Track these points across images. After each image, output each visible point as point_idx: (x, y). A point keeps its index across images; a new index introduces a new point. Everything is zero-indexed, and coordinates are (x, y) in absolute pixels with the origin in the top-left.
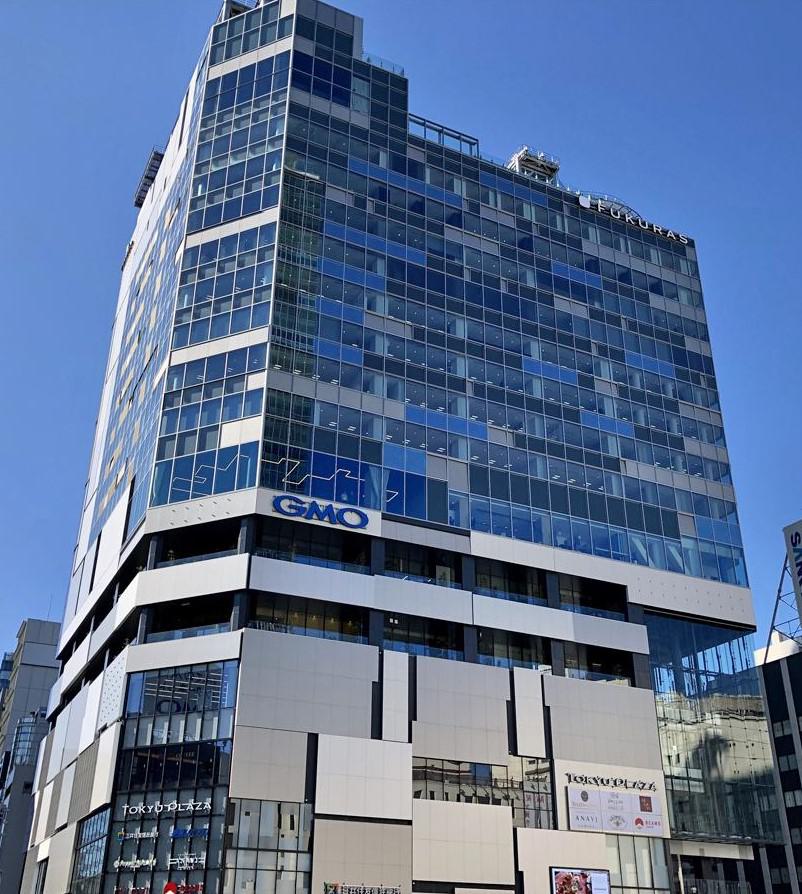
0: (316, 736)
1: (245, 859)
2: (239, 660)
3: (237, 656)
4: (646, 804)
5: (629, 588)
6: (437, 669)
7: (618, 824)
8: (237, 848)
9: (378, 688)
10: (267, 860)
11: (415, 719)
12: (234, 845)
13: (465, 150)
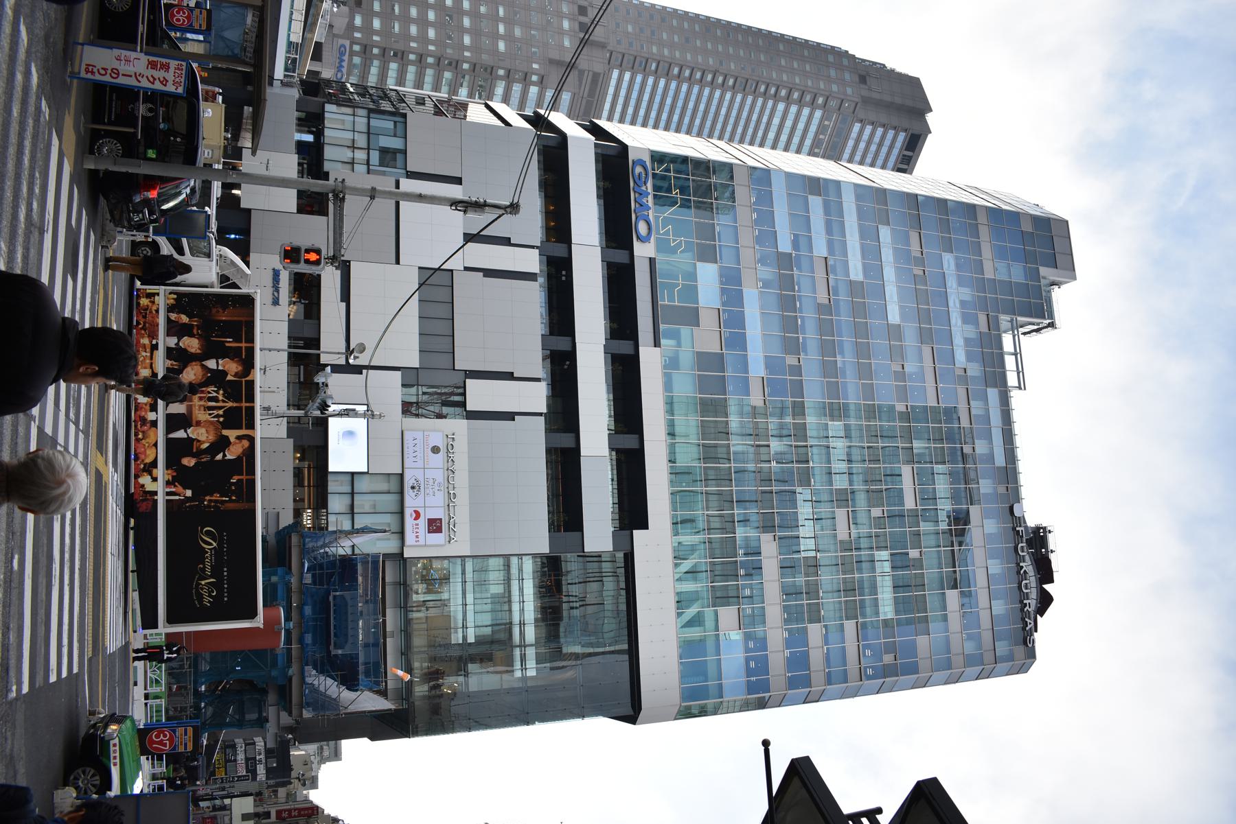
0: (460, 183)
1: (361, 122)
2: (454, 369)
3: (456, 368)
4: (434, 526)
5: (938, 778)
6: (533, 297)
7: (413, 488)
8: (369, 118)
9: (489, 273)
10: (361, 141)
11: (484, 276)
12: (372, 115)
13: (1012, 379)
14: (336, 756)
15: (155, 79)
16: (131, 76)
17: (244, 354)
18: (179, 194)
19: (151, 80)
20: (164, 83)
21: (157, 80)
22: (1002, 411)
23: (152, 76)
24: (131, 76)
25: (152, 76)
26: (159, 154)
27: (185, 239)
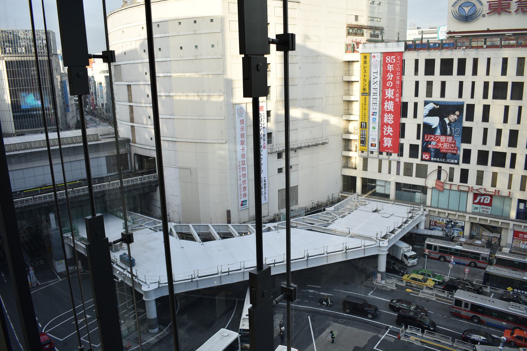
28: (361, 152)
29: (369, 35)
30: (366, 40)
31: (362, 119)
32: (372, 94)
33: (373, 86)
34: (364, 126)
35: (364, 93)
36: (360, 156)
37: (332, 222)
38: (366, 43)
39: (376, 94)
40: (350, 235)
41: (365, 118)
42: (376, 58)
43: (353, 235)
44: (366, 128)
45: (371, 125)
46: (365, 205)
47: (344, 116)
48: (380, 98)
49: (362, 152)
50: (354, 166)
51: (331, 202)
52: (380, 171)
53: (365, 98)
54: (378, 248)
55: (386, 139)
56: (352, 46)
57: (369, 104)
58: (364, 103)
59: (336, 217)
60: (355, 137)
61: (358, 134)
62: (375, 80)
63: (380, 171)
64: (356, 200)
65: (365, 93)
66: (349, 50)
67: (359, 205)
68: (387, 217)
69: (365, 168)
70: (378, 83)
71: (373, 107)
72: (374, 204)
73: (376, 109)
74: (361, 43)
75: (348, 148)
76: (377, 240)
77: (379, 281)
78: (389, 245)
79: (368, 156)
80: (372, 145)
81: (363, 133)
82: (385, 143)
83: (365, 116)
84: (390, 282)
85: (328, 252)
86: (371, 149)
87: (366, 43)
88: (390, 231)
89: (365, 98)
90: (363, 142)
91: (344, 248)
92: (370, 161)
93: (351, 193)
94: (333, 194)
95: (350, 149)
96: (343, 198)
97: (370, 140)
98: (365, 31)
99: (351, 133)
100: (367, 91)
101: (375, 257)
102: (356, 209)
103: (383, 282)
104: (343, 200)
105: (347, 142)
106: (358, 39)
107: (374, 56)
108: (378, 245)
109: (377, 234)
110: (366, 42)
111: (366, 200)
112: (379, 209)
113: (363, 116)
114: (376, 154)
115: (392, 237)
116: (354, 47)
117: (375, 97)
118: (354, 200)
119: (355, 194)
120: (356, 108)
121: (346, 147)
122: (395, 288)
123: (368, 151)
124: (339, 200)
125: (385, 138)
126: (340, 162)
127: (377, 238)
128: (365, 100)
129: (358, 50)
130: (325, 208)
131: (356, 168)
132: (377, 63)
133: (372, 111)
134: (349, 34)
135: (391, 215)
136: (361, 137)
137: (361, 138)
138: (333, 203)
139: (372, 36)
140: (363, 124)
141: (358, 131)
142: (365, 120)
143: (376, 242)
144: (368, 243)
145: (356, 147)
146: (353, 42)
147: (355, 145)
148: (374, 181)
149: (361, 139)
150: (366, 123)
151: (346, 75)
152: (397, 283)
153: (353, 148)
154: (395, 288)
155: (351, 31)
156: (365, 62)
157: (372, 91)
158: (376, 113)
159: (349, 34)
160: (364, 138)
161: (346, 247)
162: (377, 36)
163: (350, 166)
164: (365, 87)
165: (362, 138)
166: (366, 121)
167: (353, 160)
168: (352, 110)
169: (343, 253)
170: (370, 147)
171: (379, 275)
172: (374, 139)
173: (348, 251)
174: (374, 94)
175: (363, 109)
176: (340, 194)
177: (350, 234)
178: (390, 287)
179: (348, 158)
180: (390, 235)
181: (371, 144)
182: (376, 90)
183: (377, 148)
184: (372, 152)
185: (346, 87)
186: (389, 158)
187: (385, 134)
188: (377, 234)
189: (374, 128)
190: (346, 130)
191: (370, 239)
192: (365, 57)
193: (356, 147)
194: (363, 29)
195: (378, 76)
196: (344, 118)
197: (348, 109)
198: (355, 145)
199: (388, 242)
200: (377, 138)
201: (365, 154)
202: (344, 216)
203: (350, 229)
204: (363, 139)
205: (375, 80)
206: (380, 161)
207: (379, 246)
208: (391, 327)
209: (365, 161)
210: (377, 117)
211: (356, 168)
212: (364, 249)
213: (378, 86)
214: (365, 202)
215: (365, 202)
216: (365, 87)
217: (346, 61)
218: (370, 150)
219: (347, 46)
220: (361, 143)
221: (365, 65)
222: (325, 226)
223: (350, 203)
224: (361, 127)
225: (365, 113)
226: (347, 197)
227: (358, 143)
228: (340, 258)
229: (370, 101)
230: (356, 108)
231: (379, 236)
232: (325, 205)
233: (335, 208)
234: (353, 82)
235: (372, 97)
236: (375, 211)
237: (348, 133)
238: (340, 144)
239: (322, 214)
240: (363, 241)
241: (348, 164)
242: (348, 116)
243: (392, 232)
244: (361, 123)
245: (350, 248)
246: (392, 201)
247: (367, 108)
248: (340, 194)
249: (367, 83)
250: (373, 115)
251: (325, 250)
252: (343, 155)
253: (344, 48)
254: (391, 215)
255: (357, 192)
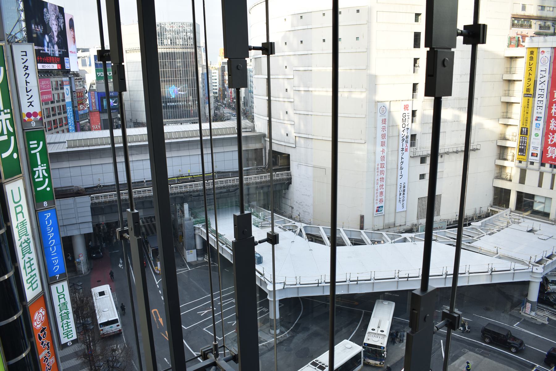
14: (263, 44)
15: (26, 74)
16: (24, 217)
17: (134, 278)
18: (262, 345)
19: (27, 75)
20: (26, 67)
21: (26, 72)
22: (363, 223)
23: (25, 75)
24: (24, 217)
25: (25, 75)
26: (282, 319)
27: (3, 155)
28: (518, 162)
29: (538, 27)
30: (534, 33)
31: (523, 124)
32: (537, 96)
33: (538, 87)
34: (524, 132)
35: (528, 94)
36: (518, 167)
37: (477, 238)
38: (533, 37)
39: (542, 96)
40: (498, 255)
41: (527, 123)
42: (545, 54)
43: (501, 256)
44: (527, 134)
45: (534, 132)
46: (519, 223)
47: (501, 120)
48: (547, 101)
49: (520, 162)
50: (508, 177)
51: (479, 217)
52: (540, 185)
53: (528, 100)
54: (531, 274)
55: (551, 148)
56: (517, 39)
57: (533, 107)
58: (527, 106)
59: (482, 233)
60: (513, 144)
61: (517, 141)
62: (542, 80)
63: (540, 185)
64: (509, 217)
65: (529, 94)
66: (512, 44)
67: (511, 222)
68: (544, 240)
69: (522, 180)
70: (546, 83)
71: (537, 111)
72: (528, 222)
73: (540, 113)
74: (528, 36)
75: (503, 157)
76: (530, 265)
77: (528, 312)
78: (544, 271)
79: (527, 167)
80: (533, 155)
81: (523, 140)
82: (549, 153)
83: (527, 120)
84: (542, 314)
85: (470, 272)
86: (531, 159)
87: (533, 37)
88: (547, 256)
89: (528, 100)
90: (522, 151)
91: (489, 270)
92: (528, 173)
93: (502, 208)
94: (481, 208)
95: (505, 158)
96: (493, 213)
97: (531, 148)
98: (533, 22)
99: (508, 140)
100: (532, 92)
101: (526, 284)
102: (507, 227)
103: (533, 314)
104: (492, 215)
105: (503, 150)
106: (525, 31)
107: (543, 52)
108: (531, 270)
109: (531, 257)
110: (534, 35)
111: (520, 218)
112: (535, 229)
113: (525, 121)
114: (537, 165)
115: (548, 263)
116: (519, 40)
117: (540, 99)
118: (506, 217)
119: (507, 210)
120: (517, 111)
121: (501, 156)
122: (547, 323)
123: (527, 161)
124: (488, 215)
125: (549, 147)
126: (493, 171)
127: (530, 263)
128: (528, 102)
129: (523, 44)
130: (470, 222)
131: (510, 180)
132: (547, 59)
133: (535, 115)
134: (513, 25)
135: (550, 237)
136: (521, 144)
137: (520, 146)
138: (480, 218)
139: (541, 27)
140: (523, 130)
141: (518, 138)
142: (526, 125)
143: (529, 266)
144: (518, 266)
145: (513, 156)
146: (517, 35)
147: (513, 153)
148: (532, 196)
149: (520, 147)
150: (527, 131)
151: (507, 72)
152: (550, 317)
153: (509, 157)
154: (547, 323)
155: (516, 22)
156: (531, 59)
157: (538, 92)
158: (541, 118)
159: (513, 25)
160: (524, 146)
161: (492, 269)
162: (549, 28)
163: (504, 176)
164: (529, 87)
165: (522, 146)
166: (528, 126)
167: (508, 171)
168: (511, 113)
169: (487, 275)
170: (530, 157)
171: (529, 305)
172: (536, 148)
173: (493, 273)
174: (540, 96)
175: (526, 112)
176: (490, 208)
177: (497, 254)
178: (540, 321)
179: (502, 168)
180: (547, 261)
181: (532, 153)
182: (543, 91)
183: (538, 158)
184: (532, 163)
185: (505, 86)
186: (552, 171)
187: (549, 143)
188: (531, 257)
189: (537, 135)
190: (503, 136)
191: (522, 262)
192: (532, 53)
193: (513, 156)
194: (531, 20)
195: (547, 75)
196: (500, 122)
197: (507, 112)
198: (513, 153)
199: (544, 268)
200: (539, 147)
201: (523, 165)
202: (493, 233)
203: (498, 249)
204: (523, 147)
205: (542, 80)
206: (541, 174)
207: (532, 272)
208: (538, 366)
209: (523, 172)
210: (541, 122)
211: (510, 180)
212: (514, 273)
213: (545, 87)
214: (519, 219)
215: (519, 219)
216: (529, 87)
217: (507, 57)
218: (529, 160)
219: (511, 39)
220: (519, 152)
221: (531, 62)
222: (469, 243)
223: (500, 219)
224: (521, 134)
225: (527, 118)
226: (497, 212)
227: (516, 152)
228: (484, 280)
229: (534, 104)
230: (517, 111)
231: (533, 261)
232: (471, 219)
233: (482, 223)
234: (514, 81)
235: (537, 99)
236: (531, 231)
237: (505, 139)
238: (494, 151)
239: (467, 229)
240: (513, 263)
241: (501, 174)
242: (507, 120)
243: (549, 257)
244: (522, 128)
245: (496, 270)
246: (551, 221)
247: (530, 112)
248: (490, 208)
249: (532, 82)
250: (537, 120)
251: (467, 270)
252: (496, 164)
253: (506, 42)
254: (550, 237)
255: (510, 207)
